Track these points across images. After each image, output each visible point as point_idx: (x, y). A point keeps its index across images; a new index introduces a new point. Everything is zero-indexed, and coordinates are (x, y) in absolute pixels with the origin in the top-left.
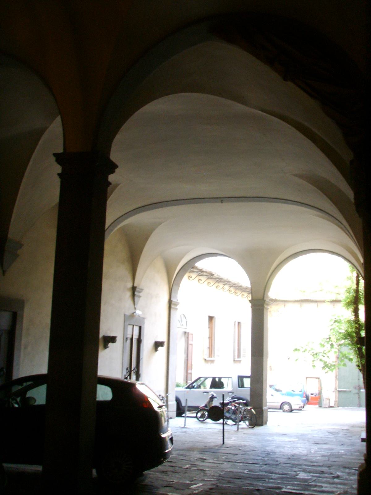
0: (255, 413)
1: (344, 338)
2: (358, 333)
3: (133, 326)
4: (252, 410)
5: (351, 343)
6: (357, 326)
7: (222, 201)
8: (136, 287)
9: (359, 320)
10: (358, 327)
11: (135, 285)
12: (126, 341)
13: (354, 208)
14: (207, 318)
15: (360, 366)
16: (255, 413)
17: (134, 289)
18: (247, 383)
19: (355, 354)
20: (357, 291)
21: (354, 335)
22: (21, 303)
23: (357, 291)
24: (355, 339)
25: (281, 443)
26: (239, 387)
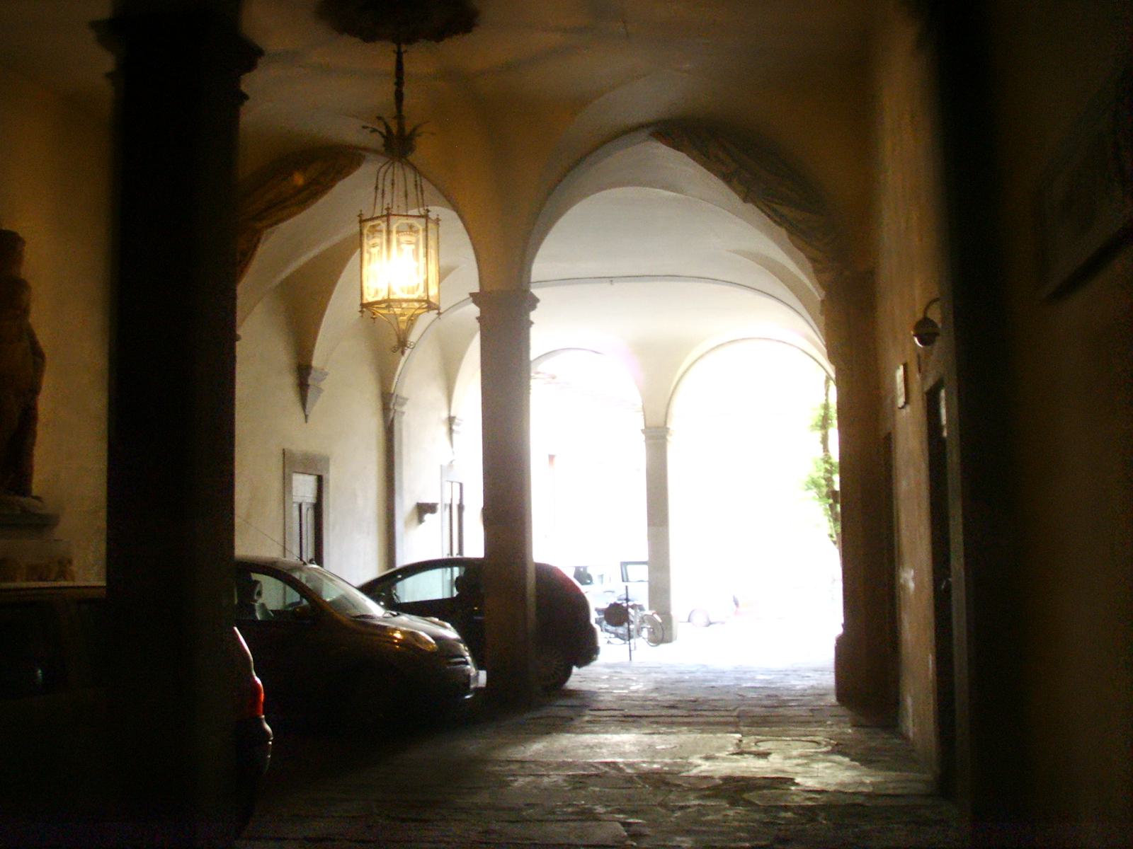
0: (660, 620)
1: (806, 487)
2: (829, 481)
3: (452, 482)
4: (656, 616)
5: (817, 497)
6: (828, 466)
7: (611, 281)
8: (454, 418)
9: (830, 458)
10: (829, 468)
11: (452, 414)
12: (445, 508)
13: (819, 306)
14: (547, 457)
15: (834, 536)
16: (660, 620)
17: (451, 420)
18: (641, 573)
19: (825, 515)
20: (826, 407)
21: (823, 482)
22: (325, 461)
23: (826, 407)
24: (825, 490)
25: (705, 674)
26: (623, 581)
